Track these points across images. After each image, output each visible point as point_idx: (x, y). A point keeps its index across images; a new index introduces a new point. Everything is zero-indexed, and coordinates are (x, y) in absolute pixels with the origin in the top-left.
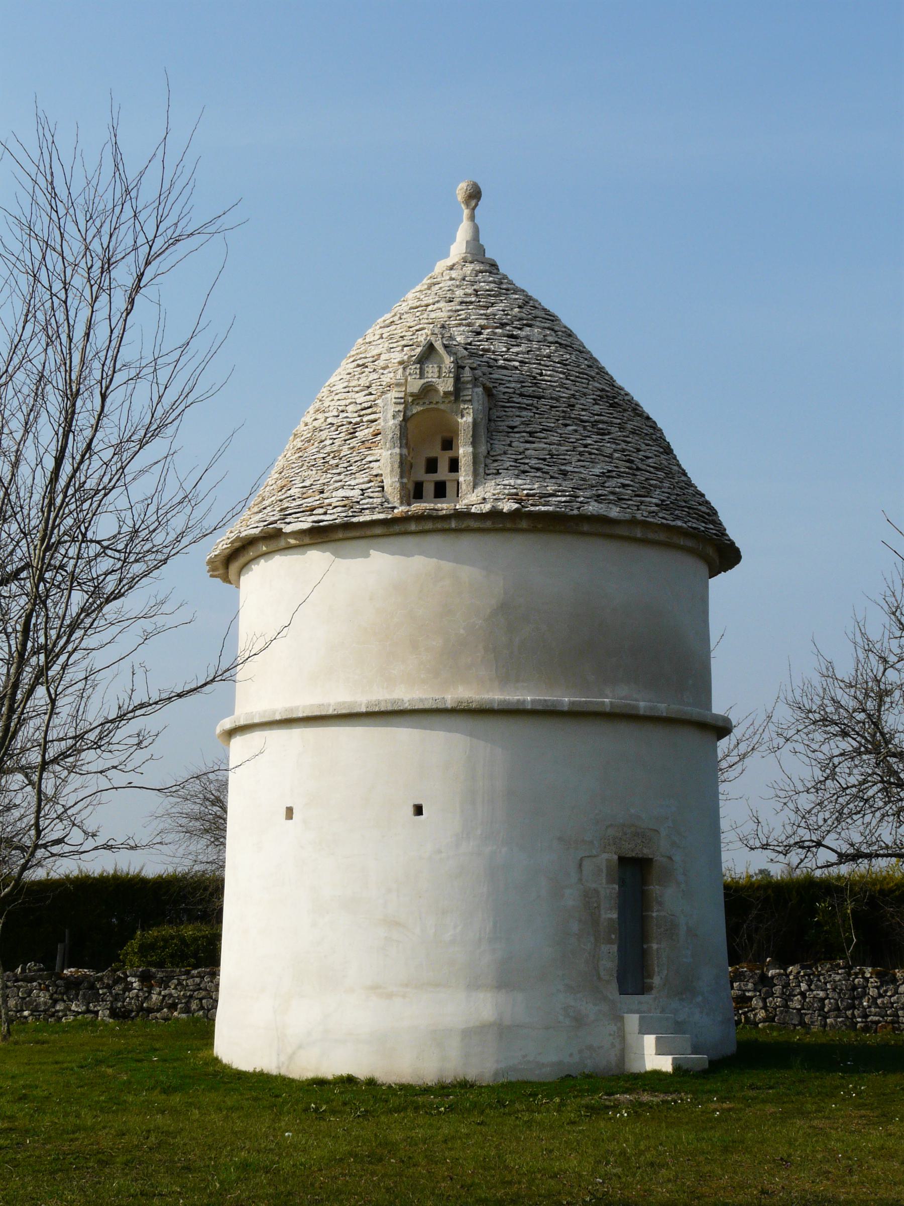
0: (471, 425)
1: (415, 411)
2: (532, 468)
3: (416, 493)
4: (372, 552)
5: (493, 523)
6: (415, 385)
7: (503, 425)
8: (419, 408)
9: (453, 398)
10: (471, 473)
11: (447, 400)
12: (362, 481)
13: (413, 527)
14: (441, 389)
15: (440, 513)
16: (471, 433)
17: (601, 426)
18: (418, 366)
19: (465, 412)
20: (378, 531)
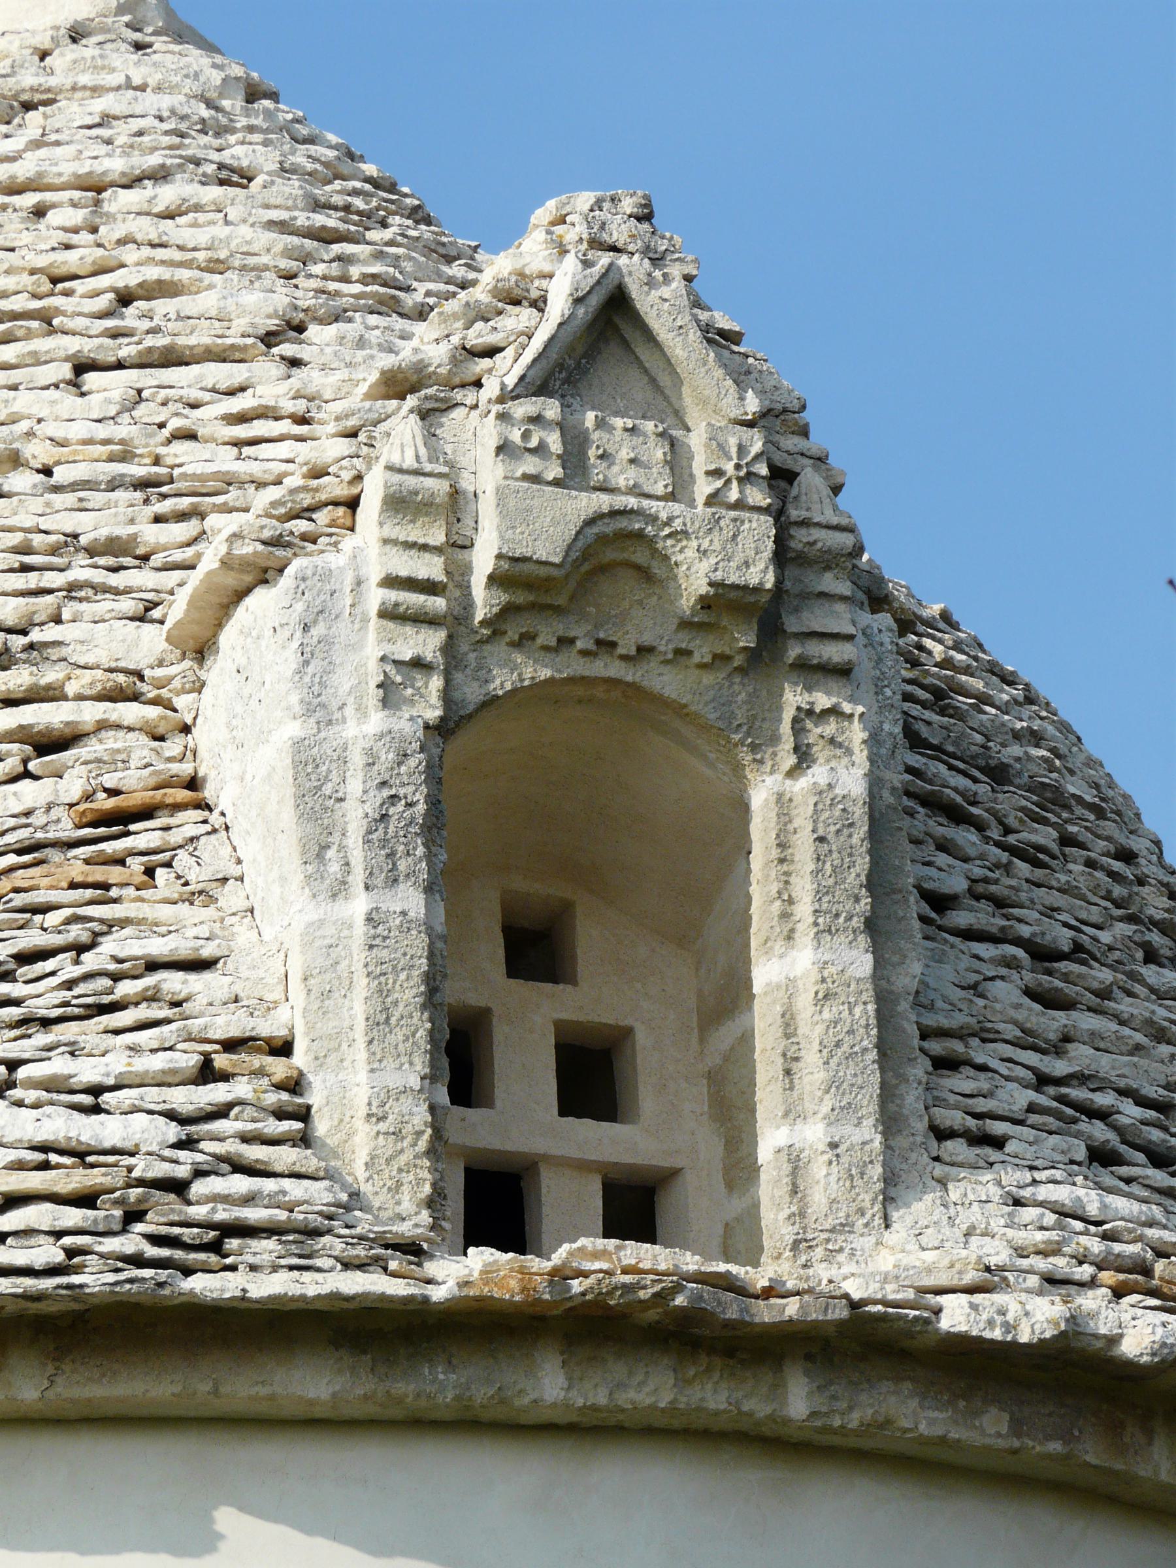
0: (859, 813)
1: (502, 681)
3: (495, 1205)
4: (226, 1519)
5: (1017, 1427)
6: (513, 519)
8: (533, 670)
9: (747, 640)
10: (869, 1106)
11: (703, 651)
12: (159, 1062)
13: (549, 1384)
14: (695, 574)
15: (766, 1313)
16: (862, 863)
18: (552, 409)
19: (815, 732)
20: (314, 1382)
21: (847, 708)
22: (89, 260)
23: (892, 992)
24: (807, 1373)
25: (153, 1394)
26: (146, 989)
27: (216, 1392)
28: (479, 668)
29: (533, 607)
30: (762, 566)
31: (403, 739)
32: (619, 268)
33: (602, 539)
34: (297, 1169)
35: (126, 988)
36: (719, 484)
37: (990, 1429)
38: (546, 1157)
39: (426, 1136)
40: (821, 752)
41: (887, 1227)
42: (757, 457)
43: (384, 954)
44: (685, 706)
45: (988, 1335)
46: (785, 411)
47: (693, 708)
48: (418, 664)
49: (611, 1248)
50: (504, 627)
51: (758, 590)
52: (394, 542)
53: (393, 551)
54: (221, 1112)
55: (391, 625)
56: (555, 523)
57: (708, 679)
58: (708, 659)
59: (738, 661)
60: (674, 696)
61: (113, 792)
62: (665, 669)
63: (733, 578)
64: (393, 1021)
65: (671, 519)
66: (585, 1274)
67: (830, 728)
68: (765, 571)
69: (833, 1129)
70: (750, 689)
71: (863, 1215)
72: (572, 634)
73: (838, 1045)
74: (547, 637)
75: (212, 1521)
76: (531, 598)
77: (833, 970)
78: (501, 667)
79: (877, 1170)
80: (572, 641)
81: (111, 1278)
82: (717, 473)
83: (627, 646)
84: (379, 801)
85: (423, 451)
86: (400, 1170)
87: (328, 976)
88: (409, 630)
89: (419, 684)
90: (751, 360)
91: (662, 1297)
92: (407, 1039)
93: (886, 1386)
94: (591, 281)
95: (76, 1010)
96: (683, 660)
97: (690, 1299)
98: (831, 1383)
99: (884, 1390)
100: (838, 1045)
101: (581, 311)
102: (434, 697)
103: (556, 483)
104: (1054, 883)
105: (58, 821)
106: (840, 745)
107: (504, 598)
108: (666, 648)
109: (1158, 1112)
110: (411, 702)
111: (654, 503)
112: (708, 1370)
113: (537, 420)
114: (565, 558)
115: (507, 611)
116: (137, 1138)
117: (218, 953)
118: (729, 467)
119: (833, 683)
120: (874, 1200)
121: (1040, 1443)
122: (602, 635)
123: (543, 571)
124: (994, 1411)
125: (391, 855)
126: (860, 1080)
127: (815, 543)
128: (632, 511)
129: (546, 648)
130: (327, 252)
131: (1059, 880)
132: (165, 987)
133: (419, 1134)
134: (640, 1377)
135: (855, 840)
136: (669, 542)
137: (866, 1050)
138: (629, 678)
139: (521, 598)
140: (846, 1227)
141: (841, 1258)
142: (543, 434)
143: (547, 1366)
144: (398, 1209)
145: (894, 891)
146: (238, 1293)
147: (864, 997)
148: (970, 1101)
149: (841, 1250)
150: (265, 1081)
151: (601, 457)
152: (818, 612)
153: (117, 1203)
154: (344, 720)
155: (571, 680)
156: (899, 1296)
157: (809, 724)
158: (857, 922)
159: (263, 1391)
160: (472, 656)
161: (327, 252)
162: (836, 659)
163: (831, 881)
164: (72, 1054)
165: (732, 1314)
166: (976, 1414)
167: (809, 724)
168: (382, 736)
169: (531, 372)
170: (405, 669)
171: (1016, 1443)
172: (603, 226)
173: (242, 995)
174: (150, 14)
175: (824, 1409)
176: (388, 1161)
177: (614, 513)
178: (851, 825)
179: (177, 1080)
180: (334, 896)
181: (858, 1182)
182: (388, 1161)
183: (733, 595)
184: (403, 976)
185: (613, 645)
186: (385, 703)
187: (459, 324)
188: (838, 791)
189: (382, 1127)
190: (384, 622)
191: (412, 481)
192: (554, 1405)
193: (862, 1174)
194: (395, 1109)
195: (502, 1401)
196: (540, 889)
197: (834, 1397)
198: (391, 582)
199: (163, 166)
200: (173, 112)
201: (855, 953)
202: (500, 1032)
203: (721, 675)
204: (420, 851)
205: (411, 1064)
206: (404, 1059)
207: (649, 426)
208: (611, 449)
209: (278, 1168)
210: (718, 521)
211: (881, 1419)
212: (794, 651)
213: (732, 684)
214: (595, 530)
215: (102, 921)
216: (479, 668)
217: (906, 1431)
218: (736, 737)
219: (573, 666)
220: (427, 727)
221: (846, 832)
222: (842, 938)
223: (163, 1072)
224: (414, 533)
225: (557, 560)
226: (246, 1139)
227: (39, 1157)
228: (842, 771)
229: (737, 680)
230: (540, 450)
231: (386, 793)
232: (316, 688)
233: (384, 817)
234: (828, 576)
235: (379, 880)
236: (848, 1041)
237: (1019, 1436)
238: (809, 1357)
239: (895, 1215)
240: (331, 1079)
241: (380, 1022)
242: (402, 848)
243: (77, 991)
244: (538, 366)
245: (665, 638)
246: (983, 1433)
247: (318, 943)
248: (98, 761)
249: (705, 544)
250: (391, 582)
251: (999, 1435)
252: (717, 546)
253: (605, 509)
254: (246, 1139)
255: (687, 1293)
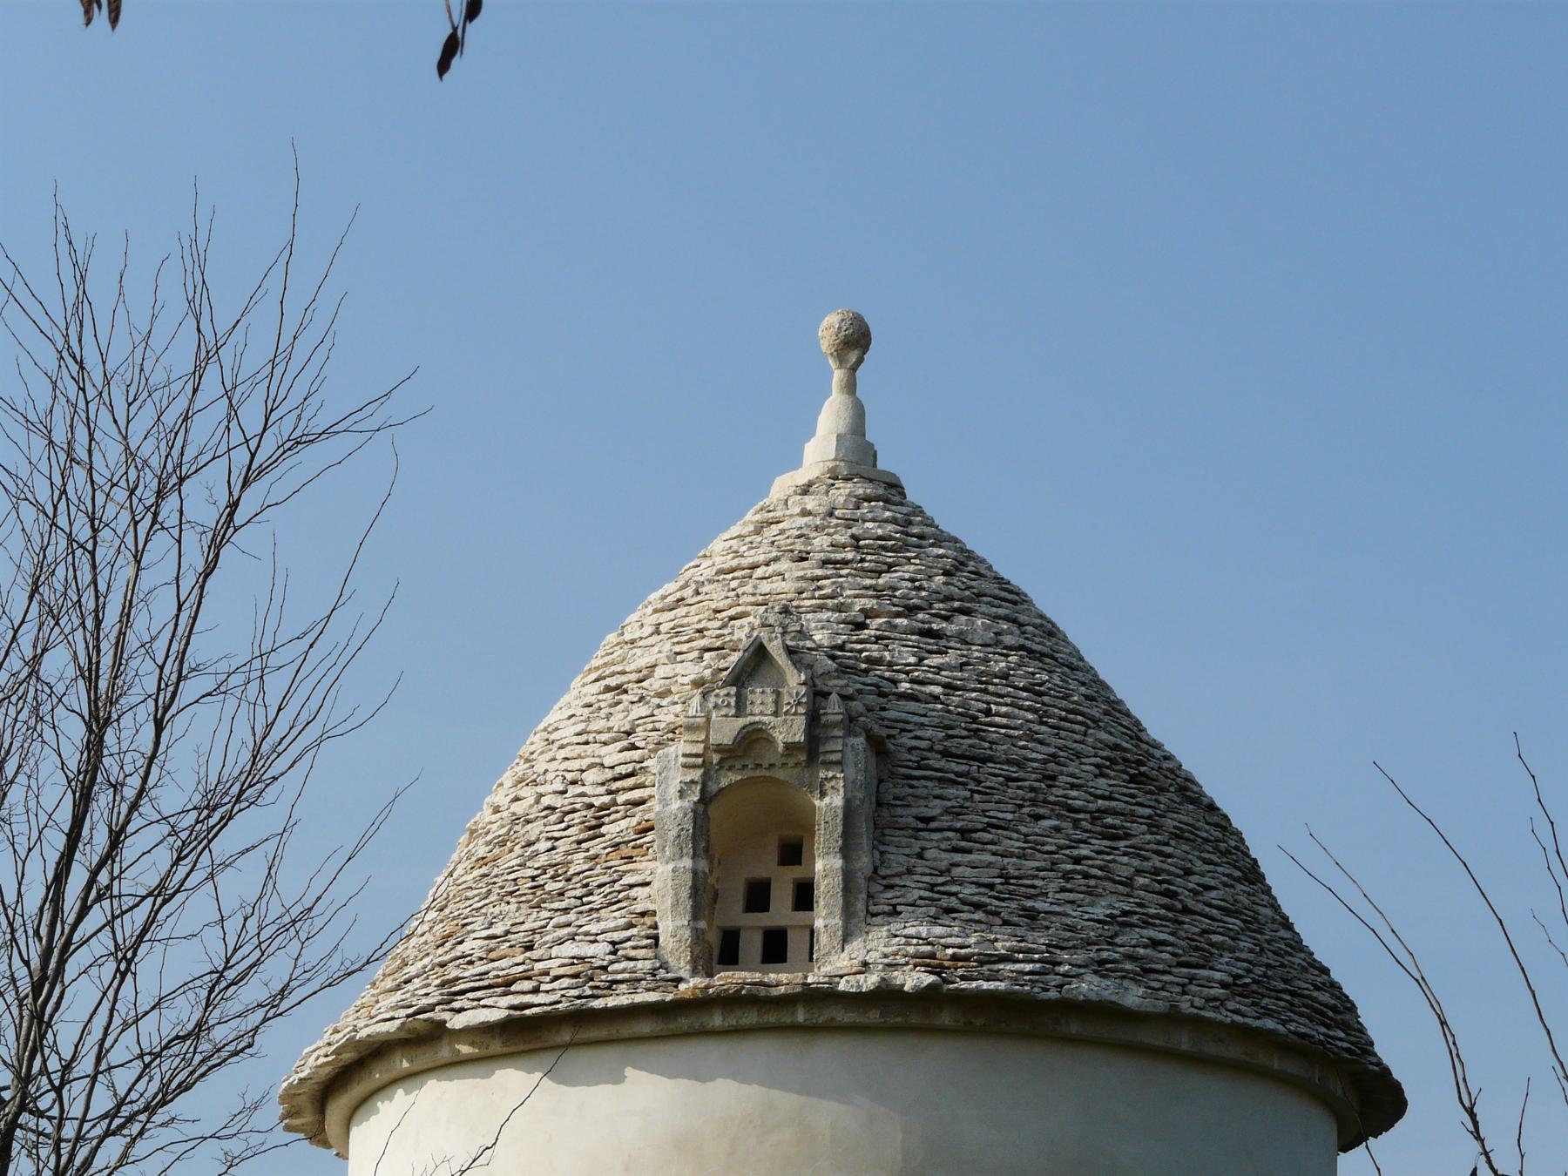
1: (724, 782)
2: (964, 902)
4: (629, 1071)
5: (882, 1016)
6: (726, 730)
7: (907, 816)
9: (803, 757)
10: (838, 911)
11: (791, 762)
13: (717, 1020)
15: (775, 992)
16: (840, 829)
17: (1109, 820)
18: (733, 690)
19: (828, 785)
20: (645, 1027)
37: (873, 1016)
48: (692, 782)
74: (738, 766)
83: (766, 765)
108: (778, 763)
109: (592, 1010)
115: (721, 761)
140: (829, 953)
194: (680, 932)
198: (685, 755)
207: (769, 690)
226: (634, 948)
241: (675, 904)
250: (685, 755)
254: (634, 948)
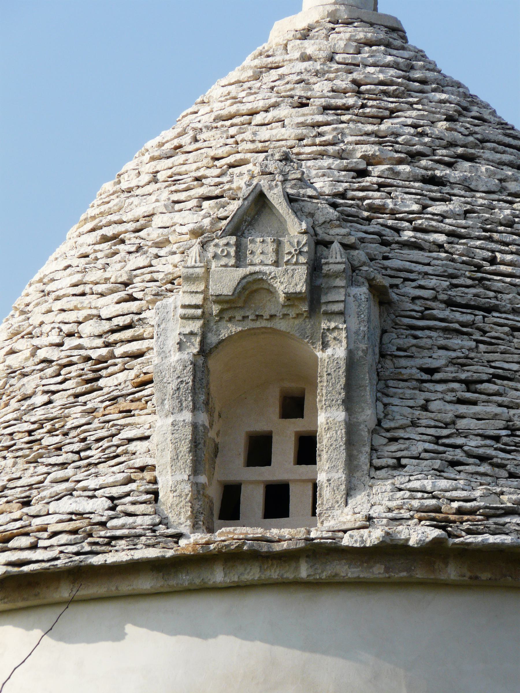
0: (343, 364)
1: (224, 334)
4: (129, 628)
5: (387, 570)
6: (226, 280)
8: (233, 328)
10: (341, 464)
11: (292, 313)
13: (218, 576)
15: (277, 547)
16: (343, 381)
18: (233, 240)
20: (145, 583)
21: (341, 326)
22: (225, 152)
23: (358, 422)
24: (307, 562)
25: (99, 592)
26: (123, 450)
27: (117, 588)
28: (217, 330)
29: (231, 308)
30: (301, 284)
31: (185, 361)
32: (260, 185)
33: (248, 283)
34: (144, 512)
35: (120, 450)
36: (290, 257)
37: (377, 571)
38: (290, 480)
39: (189, 496)
40: (332, 343)
41: (346, 506)
42: (304, 245)
43: (177, 436)
44: (289, 333)
45: (355, 545)
46: (331, 220)
47: (291, 333)
49: (232, 531)
50: (224, 316)
51: (300, 293)
52: (187, 292)
53: (186, 295)
54: (128, 494)
55: (185, 321)
56: (230, 281)
57: (297, 322)
58: (294, 316)
59: (305, 314)
60: (284, 330)
61: (145, 374)
62: (280, 321)
63: (291, 291)
64: (179, 458)
65: (270, 273)
66: (214, 542)
67: (335, 334)
68: (302, 286)
69: (328, 475)
70: (312, 323)
71: (338, 503)
72: (247, 315)
73: (331, 445)
75: (124, 629)
76: (229, 306)
77: (331, 419)
78: (224, 329)
79: (343, 487)
80: (248, 317)
81: (67, 560)
82: (290, 253)
83: (266, 316)
84: (177, 383)
85: (198, 258)
86: (181, 508)
87: (164, 444)
88: (190, 322)
89: (193, 340)
90: (319, 205)
91: (240, 547)
92: (184, 463)
93: (336, 563)
94: (249, 192)
95: (103, 460)
96: (287, 317)
97: (248, 547)
98: (315, 564)
99: (335, 564)
100: (331, 445)
101: (246, 202)
102: (197, 346)
103: (233, 266)
104: (498, 350)
105: (128, 386)
106: (338, 340)
107: (220, 307)
110: (189, 347)
111: (267, 268)
112: (272, 565)
113: (228, 244)
114: (233, 293)
115: (222, 311)
116: (95, 508)
117: (150, 434)
118: (293, 250)
119: (338, 318)
120: (341, 498)
121: (397, 574)
122: (257, 313)
123: (227, 298)
124: (378, 565)
125: (181, 402)
126: (338, 457)
127: (330, 270)
128: (257, 272)
129: (239, 321)
130: (312, 133)
131: (500, 349)
132: (129, 449)
133: (187, 495)
134: (248, 571)
135: (341, 373)
136: (272, 280)
137: (341, 446)
138: (269, 326)
139: (225, 306)
141: (330, 518)
142: (229, 249)
143: (218, 570)
144: (180, 521)
145: (360, 387)
146: (103, 562)
147: (341, 427)
148: (394, 454)
149: (329, 516)
150: (145, 481)
151: (251, 254)
152: (333, 293)
153: (84, 531)
154: (171, 355)
155: (249, 329)
156: (326, 535)
157: (328, 334)
158: (339, 402)
159: (130, 588)
160: (215, 326)
161: (312, 133)
162: (336, 310)
163: (331, 389)
164: (97, 476)
165: (265, 549)
166: (371, 567)
167: (328, 334)
168: (178, 361)
169: (227, 228)
170: (188, 336)
171: (387, 575)
172: (266, 166)
173: (151, 449)
174: (342, 14)
175: (312, 573)
176: (177, 506)
177: (251, 274)
178: (339, 368)
179: (119, 484)
180: (167, 416)
181: (336, 492)
182: (177, 506)
183: (293, 295)
184: (183, 442)
185: (262, 316)
186: (180, 349)
187: (216, 210)
188: (336, 356)
189: (175, 494)
190: (183, 320)
191: (191, 271)
192: (220, 583)
193: (338, 489)
194: (179, 487)
195: (205, 583)
196: (291, 385)
197: (316, 569)
198: (184, 307)
199: (276, 102)
200: (306, 69)
201: (338, 412)
202: (275, 439)
203: (301, 320)
204: (190, 399)
205: (185, 471)
206: (183, 470)
208: (254, 250)
209: (138, 513)
210: (287, 271)
211: (333, 574)
212: (323, 308)
213: (306, 322)
214: (245, 280)
215: (121, 425)
216: (217, 330)
217: (344, 577)
218: (306, 340)
219: (249, 325)
220: (194, 355)
221: (337, 370)
222: (334, 408)
223: (113, 482)
224: (194, 288)
225: (230, 294)
227: (69, 516)
228: (337, 349)
229: (307, 320)
230: (228, 255)
231: (179, 380)
232: (162, 346)
233: (178, 389)
234: (338, 279)
235: (176, 411)
236: (335, 443)
237: (387, 573)
238: (308, 556)
239: (350, 501)
240: (164, 478)
241: (175, 458)
242: (184, 398)
243: (107, 452)
244: (230, 225)
245: (278, 311)
246: (373, 573)
247: (162, 433)
248: (143, 363)
249: (282, 280)
250: (184, 307)
251: (380, 573)
252: (286, 280)
253: (248, 273)
254: (134, 503)
255: (248, 545)
